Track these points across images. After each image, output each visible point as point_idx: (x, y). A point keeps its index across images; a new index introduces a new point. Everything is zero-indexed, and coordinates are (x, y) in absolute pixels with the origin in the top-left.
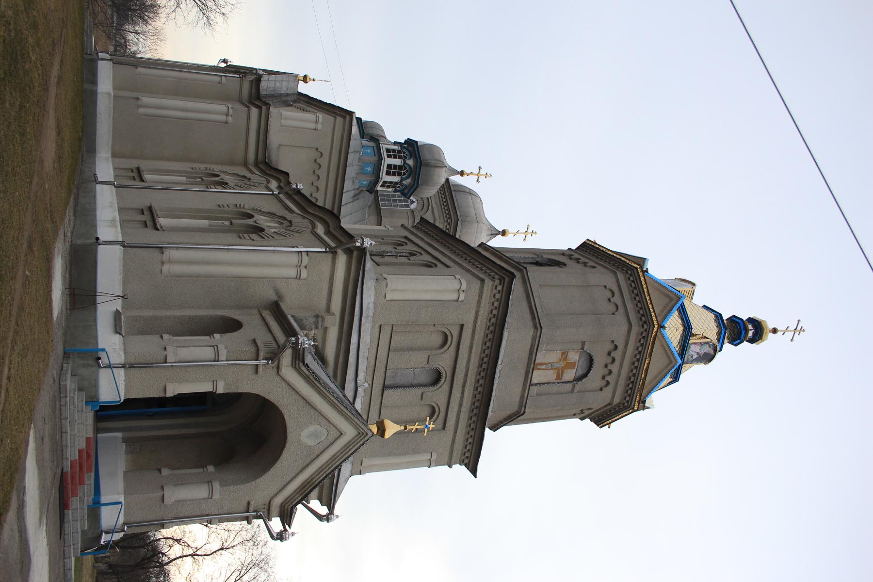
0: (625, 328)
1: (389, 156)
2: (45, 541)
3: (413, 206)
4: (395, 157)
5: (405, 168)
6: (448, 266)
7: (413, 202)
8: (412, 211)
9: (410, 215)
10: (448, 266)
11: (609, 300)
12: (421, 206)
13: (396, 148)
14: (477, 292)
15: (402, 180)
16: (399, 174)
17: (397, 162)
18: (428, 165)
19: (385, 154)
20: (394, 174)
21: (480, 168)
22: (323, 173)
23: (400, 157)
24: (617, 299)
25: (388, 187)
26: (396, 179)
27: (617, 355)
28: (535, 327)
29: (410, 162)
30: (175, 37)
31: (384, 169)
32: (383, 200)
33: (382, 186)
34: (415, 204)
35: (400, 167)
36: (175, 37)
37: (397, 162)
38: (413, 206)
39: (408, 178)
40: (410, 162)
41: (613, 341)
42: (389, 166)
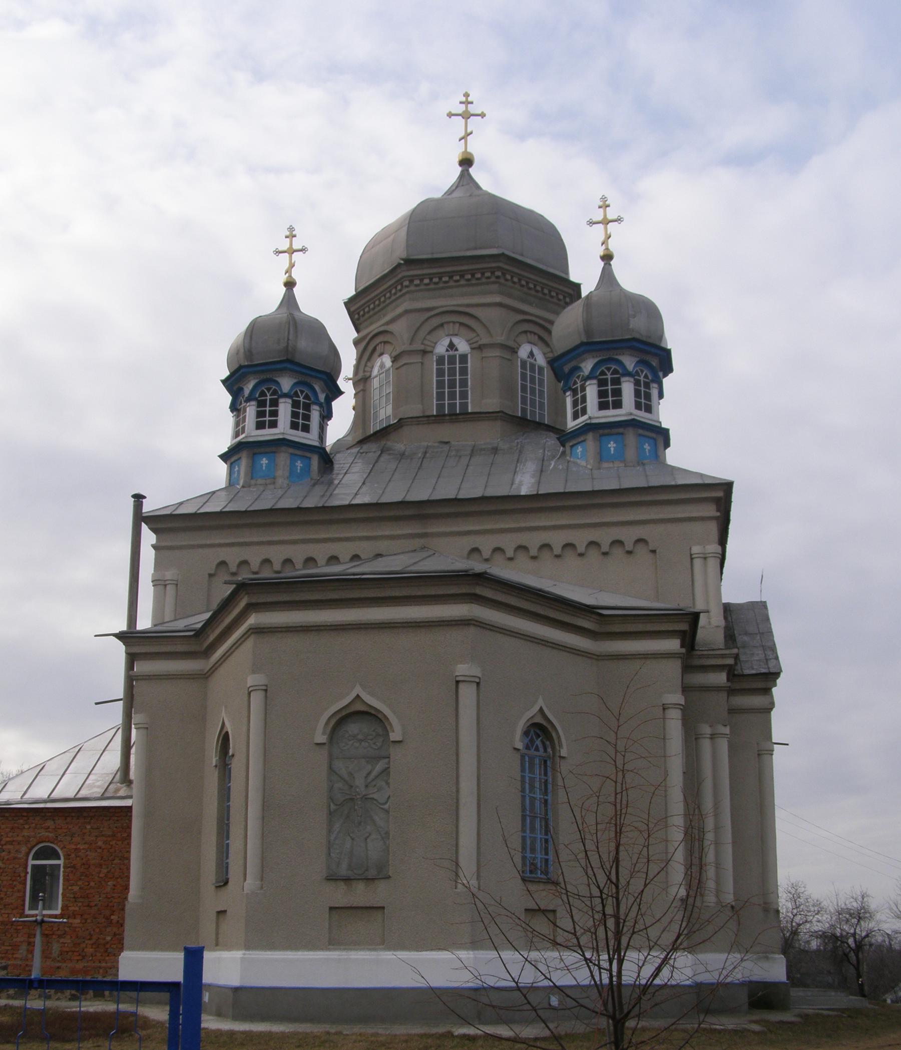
3: (463, 347)
5: (603, 373)
6: (225, 739)
7: (452, 346)
10: (225, 739)
13: (251, 411)
14: (225, 665)
15: (628, 374)
16: (307, 407)
17: (285, 409)
18: (588, 331)
20: (307, 418)
21: (591, 223)
22: (605, 537)
23: (275, 403)
26: (628, 389)
28: (469, 624)
29: (587, 366)
31: (611, 415)
34: (456, 341)
35: (602, 383)
38: (463, 347)
39: (620, 363)
42: (603, 406)
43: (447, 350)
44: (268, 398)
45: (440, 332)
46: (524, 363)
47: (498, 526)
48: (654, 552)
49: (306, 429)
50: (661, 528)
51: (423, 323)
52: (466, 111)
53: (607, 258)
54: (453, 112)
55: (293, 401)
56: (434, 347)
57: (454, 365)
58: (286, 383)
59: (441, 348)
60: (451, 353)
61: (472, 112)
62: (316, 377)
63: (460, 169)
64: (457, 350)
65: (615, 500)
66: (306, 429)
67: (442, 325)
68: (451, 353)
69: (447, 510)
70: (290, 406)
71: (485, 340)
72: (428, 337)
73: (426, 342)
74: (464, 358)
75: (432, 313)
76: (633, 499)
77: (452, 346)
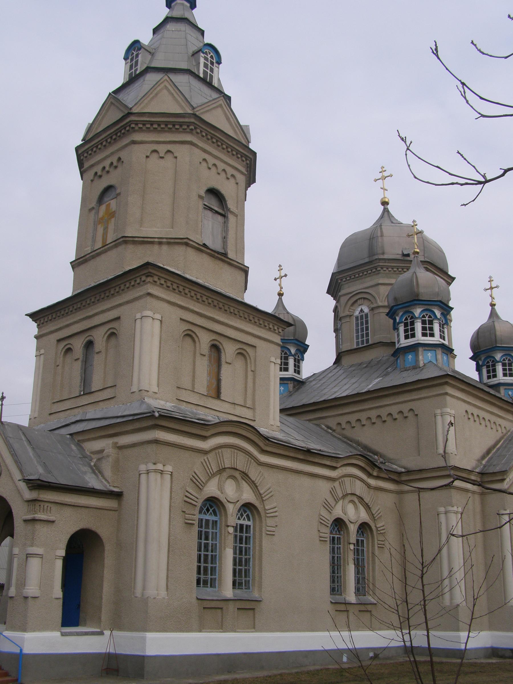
0: (136, 147)
1: (413, 336)
2: (104, 591)
3: (366, 310)
4: (413, 329)
7: (362, 311)
8: (372, 309)
9: (376, 311)
11: (162, 158)
12: (366, 301)
16: (431, 323)
17: (418, 326)
19: (428, 338)
20: (431, 329)
24: (162, 149)
25: (443, 332)
27: (98, 169)
30: (20, 411)
32: (367, 341)
33: (444, 339)
36: (20, 411)
37: (418, 326)
38: (366, 310)
40: (417, 311)
41: (92, 181)
43: (359, 313)
44: (409, 321)
45: (356, 305)
46: (357, 318)
47: (397, 401)
48: (417, 415)
49: (432, 335)
50: (418, 403)
51: (348, 300)
52: (383, 176)
53: (280, 295)
54: (377, 178)
55: (422, 320)
56: (354, 312)
57: (363, 319)
58: (417, 311)
59: (357, 313)
60: (361, 314)
61: (386, 176)
62: (288, 343)
63: (383, 207)
64: (364, 312)
65: (415, 387)
66: (432, 335)
67: (356, 301)
68: (361, 314)
69: (391, 392)
70: (420, 323)
71: (375, 305)
72: (351, 308)
73: (350, 310)
74: (366, 315)
75: (351, 295)
76: (435, 382)
77: (362, 311)
